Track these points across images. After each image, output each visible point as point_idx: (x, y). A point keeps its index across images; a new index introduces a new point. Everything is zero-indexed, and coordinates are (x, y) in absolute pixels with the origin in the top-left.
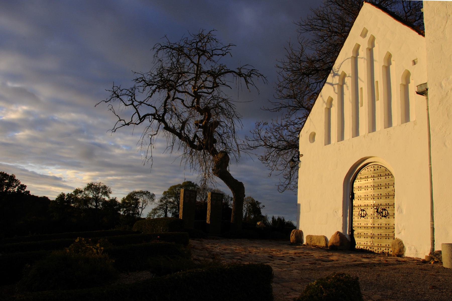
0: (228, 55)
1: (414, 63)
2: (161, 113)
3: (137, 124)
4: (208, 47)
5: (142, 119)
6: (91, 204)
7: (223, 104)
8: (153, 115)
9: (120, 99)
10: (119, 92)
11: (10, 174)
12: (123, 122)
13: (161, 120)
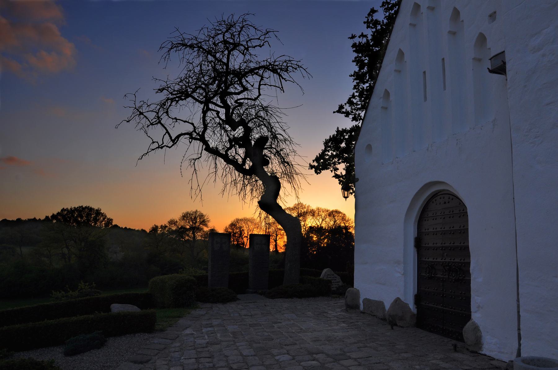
0: (266, 44)
1: (493, 16)
2: (200, 130)
3: (170, 147)
4: (243, 39)
5: (175, 141)
6: (188, 235)
7: (262, 114)
8: (190, 134)
9: (145, 116)
10: (144, 110)
11: (96, 208)
12: (156, 145)
13: (202, 139)
